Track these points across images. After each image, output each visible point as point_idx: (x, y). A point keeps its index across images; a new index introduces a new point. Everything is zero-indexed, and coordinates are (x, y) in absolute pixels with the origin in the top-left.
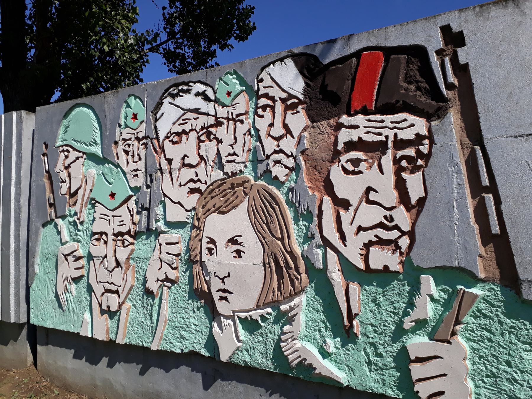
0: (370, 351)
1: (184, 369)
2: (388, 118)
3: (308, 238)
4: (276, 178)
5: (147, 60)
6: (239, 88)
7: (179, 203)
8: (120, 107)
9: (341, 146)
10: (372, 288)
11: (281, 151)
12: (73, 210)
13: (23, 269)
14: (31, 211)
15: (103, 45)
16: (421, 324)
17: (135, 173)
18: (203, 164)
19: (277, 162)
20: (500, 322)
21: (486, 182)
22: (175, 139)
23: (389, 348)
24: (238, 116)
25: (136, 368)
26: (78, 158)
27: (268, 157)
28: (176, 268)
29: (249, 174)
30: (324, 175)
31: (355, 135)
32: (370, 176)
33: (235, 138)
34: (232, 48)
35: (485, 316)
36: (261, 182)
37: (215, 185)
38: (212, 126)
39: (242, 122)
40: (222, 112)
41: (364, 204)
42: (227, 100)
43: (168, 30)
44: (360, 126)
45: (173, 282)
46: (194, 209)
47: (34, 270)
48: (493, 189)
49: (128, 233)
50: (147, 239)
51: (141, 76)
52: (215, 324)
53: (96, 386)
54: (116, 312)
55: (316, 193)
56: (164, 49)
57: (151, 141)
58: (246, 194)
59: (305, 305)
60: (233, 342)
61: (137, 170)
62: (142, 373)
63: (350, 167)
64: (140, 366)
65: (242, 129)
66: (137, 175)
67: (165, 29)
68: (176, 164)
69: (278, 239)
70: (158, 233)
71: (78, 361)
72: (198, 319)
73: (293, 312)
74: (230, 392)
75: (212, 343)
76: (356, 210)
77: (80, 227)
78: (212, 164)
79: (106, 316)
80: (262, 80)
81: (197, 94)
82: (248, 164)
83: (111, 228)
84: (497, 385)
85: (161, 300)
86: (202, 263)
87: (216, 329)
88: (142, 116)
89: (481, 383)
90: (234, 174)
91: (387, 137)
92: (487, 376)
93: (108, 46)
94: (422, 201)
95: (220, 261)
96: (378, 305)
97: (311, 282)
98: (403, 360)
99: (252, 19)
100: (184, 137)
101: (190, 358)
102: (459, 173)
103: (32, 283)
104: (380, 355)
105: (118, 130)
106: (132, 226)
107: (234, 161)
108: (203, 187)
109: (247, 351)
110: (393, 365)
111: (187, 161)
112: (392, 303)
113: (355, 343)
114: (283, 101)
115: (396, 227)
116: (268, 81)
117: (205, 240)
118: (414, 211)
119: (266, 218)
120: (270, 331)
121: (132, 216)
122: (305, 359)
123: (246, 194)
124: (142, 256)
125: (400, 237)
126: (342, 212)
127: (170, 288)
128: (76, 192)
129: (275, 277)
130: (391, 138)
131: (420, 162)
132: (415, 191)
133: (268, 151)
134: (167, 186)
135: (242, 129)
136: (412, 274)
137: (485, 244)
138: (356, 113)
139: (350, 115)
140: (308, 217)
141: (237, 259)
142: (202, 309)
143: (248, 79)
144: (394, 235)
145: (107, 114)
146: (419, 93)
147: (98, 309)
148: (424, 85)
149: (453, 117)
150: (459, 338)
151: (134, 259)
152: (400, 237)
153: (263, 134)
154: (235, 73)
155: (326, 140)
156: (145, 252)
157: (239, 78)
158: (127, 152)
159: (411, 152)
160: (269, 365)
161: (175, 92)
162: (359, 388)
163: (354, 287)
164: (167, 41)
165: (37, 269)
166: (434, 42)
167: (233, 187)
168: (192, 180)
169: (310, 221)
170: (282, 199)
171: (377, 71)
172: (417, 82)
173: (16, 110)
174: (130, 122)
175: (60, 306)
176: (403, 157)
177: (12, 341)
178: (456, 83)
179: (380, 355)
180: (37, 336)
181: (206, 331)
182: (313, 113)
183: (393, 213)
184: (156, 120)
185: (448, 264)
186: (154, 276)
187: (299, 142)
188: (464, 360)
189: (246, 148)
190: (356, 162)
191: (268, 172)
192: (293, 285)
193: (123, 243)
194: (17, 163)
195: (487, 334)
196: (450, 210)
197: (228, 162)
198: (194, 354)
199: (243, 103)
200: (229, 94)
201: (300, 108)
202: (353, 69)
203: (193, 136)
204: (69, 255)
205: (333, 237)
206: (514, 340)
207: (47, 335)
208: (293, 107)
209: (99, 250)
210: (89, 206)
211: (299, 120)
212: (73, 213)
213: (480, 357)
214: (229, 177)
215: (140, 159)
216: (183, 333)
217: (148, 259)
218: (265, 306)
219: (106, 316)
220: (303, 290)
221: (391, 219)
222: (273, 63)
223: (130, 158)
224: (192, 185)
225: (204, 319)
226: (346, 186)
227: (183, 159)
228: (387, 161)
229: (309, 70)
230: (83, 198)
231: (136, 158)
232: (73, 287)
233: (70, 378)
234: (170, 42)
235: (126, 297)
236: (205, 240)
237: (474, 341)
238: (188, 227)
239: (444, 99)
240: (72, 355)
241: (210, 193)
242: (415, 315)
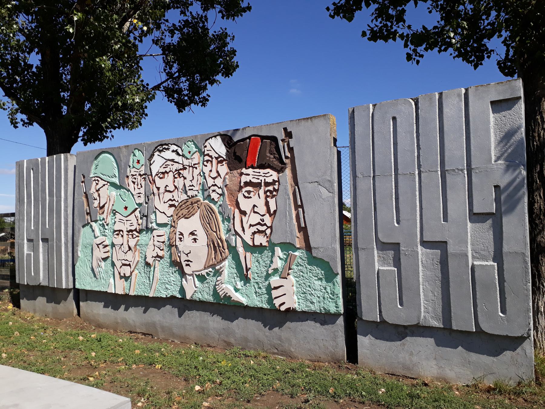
0: (256, 286)
1: (168, 307)
2: (262, 171)
3: (229, 231)
4: (213, 199)
6: (195, 150)
7: (164, 213)
8: (130, 155)
9: (242, 184)
10: (256, 255)
11: (215, 185)
12: (102, 217)
13: (70, 255)
14: (75, 217)
15: (118, 101)
16: (276, 270)
17: (139, 195)
18: (176, 190)
19: (214, 191)
20: (306, 268)
21: (299, 203)
22: (161, 176)
23: (264, 284)
24: (194, 165)
25: (141, 309)
26: (104, 185)
27: (209, 188)
28: (162, 250)
29: (200, 197)
30: (236, 198)
32: (255, 200)
33: (193, 177)
34: (220, 83)
35: (301, 265)
36: (206, 201)
37: (183, 202)
38: (181, 169)
39: (196, 168)
40: (186, 162)
41: (252, 213)
42: (188, 156)
43: (167, 71)
44: (250, 174)
45: (161, 258)
46: (172, 216)
47: (77, 255)
48: (302, 206)
49: (135, 230)
50: (146, 233)
52: (184, 280)
53: (117, 323)
54: (129, 277)
55: (232, 208)
56: (164, 87)
57: (147, 176)
58: (199, 208)
59: (227, 266)
60: (193, 289)
61: (140, 193)
62: (145, 312)
63: (246, 195)
64: (144, 308)
65: (196, 172)
66: (140, 196)
67: (165, 70)
68: (162, 190)
69: (214, 232)
70: (152, 230)
71: (106, 309)
72: (175, 277)
73: (222, 270)
74: (192, 317)
75: (182, 290)
76: (249, 216)
77: (106, 227)
78: (181, 191)
79: (123, 279)
80: (206, 147)
81: (173, 151)
82: (200, 191)
83: (125, 227)
84: (305, 297)
85: (154, 268)
86: (176, 246)
87: (184, 281)
88: (142, 162)
89: (300, 297)
90: (192, 197)
91: (261, 180)
92: (302, 293)
93: (121, 102)
94: (275, 212)
95: (185, 245)
96: (259, 263)
97: (230, 253)
98: (269, 289)
99: (235, 59)
100: (166, 175)
101: (171, 300)
102: (289, 199)
103: (77, 262)
104: (260, 288)
105: (128, 169)
106: (138, 226)
107: (192, 189)
108: (176, 204)
109: (200, 292)
110: (265, 292)
111: (168, 189)
112: (264, 262)
113: (250, 283)
114: (217, 158)
115: (265, 224)
117: (178, 233)
118: (273, 216)
119: (208, 221)
120: (212, 280)
121: (137, 220)
122: (227, 293)
123: (199, 208)
124: (143, 244)
125: (266, 229)
126: (243, 217)
127: (159, 261)
128: (104, 206)
129: (213, 252)
130: (263, 181)
131: (274, 193)
132: (273, 208)
133: (209, 185)
134: (157, 202)
135: (196, 172)
136: (272, 246)
137: (299, 232)
138: (249, 168)
139: (246, 169)
140: (228, 220)
141: (195, 243)
142: (177, 272)
143: (199, 145)
144: (264, 228)
145: (122, 159)
146: (274, 160)
147: (118, 276)
148: (277, 156)
149: (288, 172)
150: (291, 277)
151: (139, 245)
152: (266, 229)
154: (193, 141)
155: (236, 180)
156: (145, 241)
157: (195, 144)
158: (134, 183)
159: (271, 188)
160: (211, 299)
161: (161, 149)
162: (252, 306)
163: (248, 255)
164: (167, 80)
165: (79, 254)
166: (280, 135)
167: (192, 204)
168: (170, 200)
169: (229, 222)
170: (216, 210)
171: (257, 147)
172: (274, 154)
173: (63, 153)
174: (136, 165)
175: (95, 276)
176: (268, 191)
177: (63, 301)
178: (289, 156)
179: (260, 288)
180: (80, 295)
181: (179, 284)
182: (230, 166)
183: (264, 217)
184: (151, 165)
185: (285, 241)
186: (150, 254)
187: (224, 181)
188: (293, 286)
189: (199, 183)
190: (249, 192)
191: (209, 196)
192: (221, 256)
193: (133, 236)
194: (65, 187)
195: (302, 274)
196: (286, 216)
197: (190, 190)
198: (173, 297)
199: (196, 159)
200: (190, 152)
201: (224, 162)
202: (247, 145)
203: (171, 174)
204: (100, 244)
205: (239, 230)
206: (311, 276)
207: (86, 295)
208: (221, 162)
209: (118, 240)
210: (112, 214)
211: (224, 169)
212: (102, 219)
213: (299, 285)
214: (190, 198)
215: (142, 187)
216: (167, 286)
217: (147, 245)
218: (209, 267)
219: (123, 279)
220: (226, 258)
221: (263, 220)
222: (211, 138)
223: (136, 186)
224: (170, 202)
225: (179, 277)
226: (245, 205)
227: (166, 187)
228: (262, 192)
229: (228, 144)
230: (108, 209)
231: (139, 186)
232: (103, 264)
233: (101, 320)
234: (169, 81)
235: (135, 268)
236: (178, 233)
237: (297, 277)
238: (169, 226)
239: (285, 164)
240: (102, 306)
241: (180, 207)
242: (273, 266)
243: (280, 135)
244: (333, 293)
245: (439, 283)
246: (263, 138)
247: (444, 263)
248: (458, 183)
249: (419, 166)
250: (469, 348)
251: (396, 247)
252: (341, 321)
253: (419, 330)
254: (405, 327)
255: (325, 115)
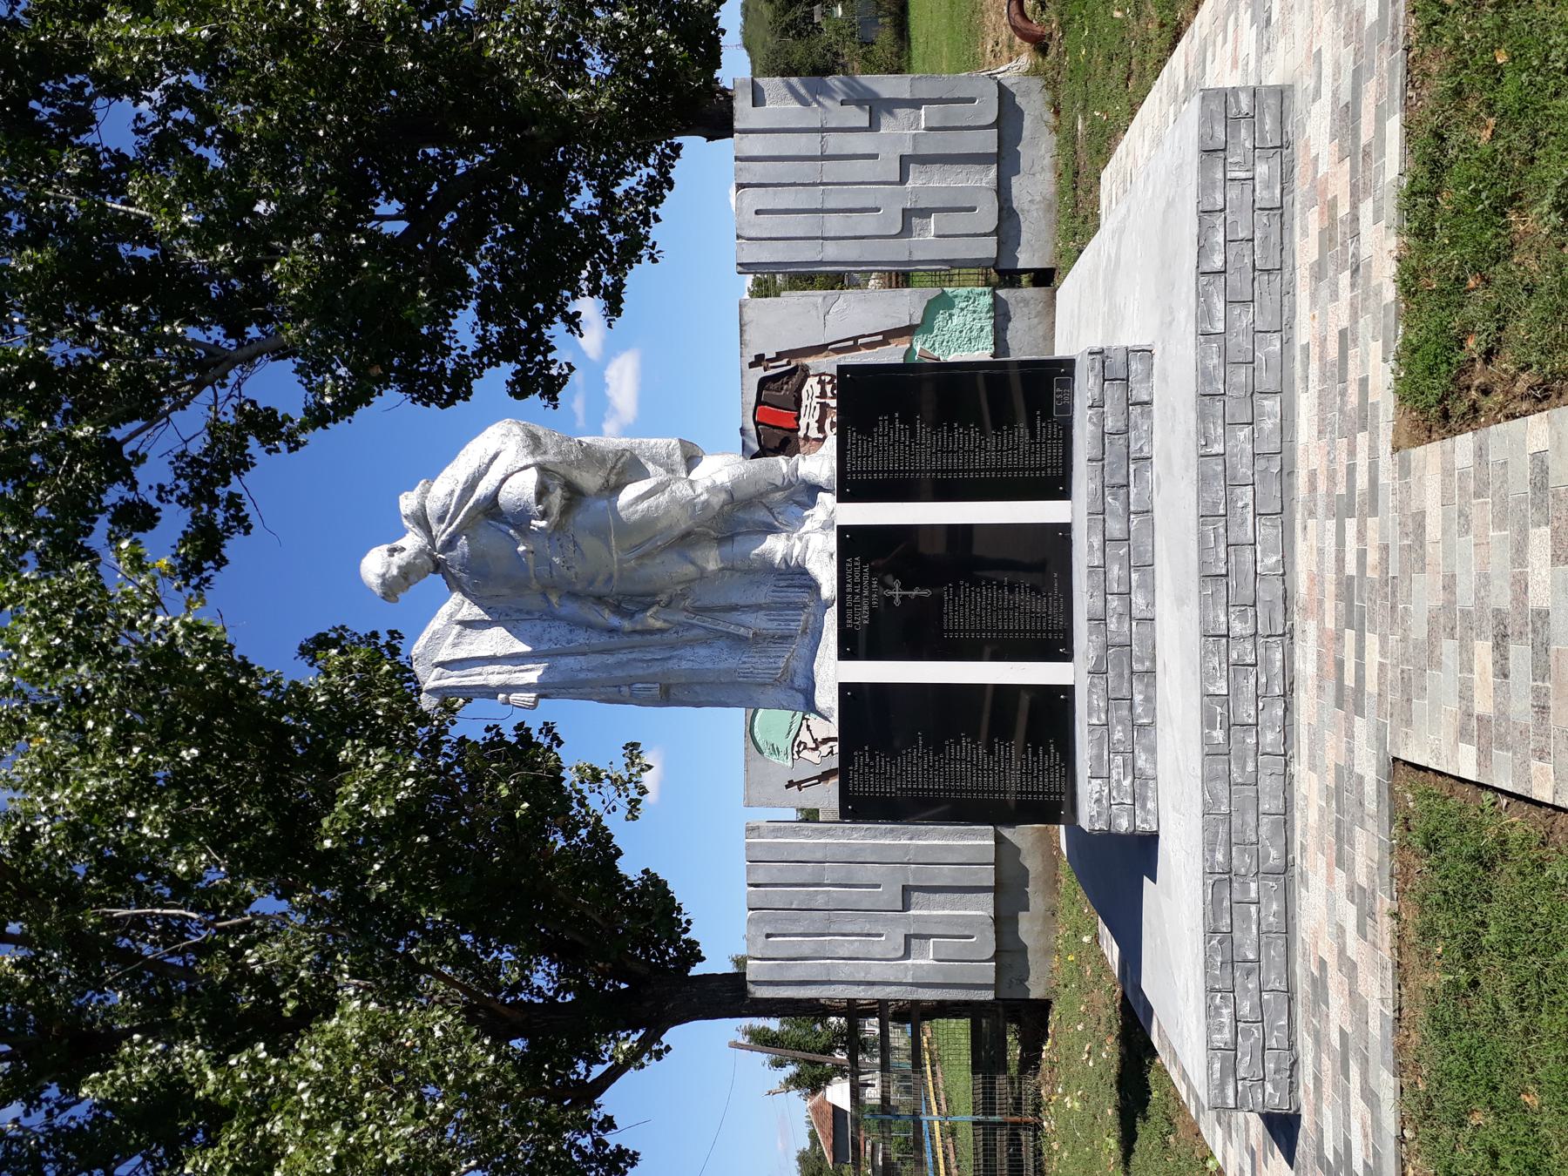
2: (805, 402)
31: (814, 425)
48: (855, 339)
166: (760, 372)
239: (796, 368)
243: (760, 372)
244: (967, 298)
245: (947, 167)
246: (759, 402)
247: (925, 160)
248: (835, 143)
249: (814, 184)
250: (1018, 138)
251: (907, 214)
252: (1007, 832)
253: (1004, 923)
254: (1000, 210)
255: (740, 306)
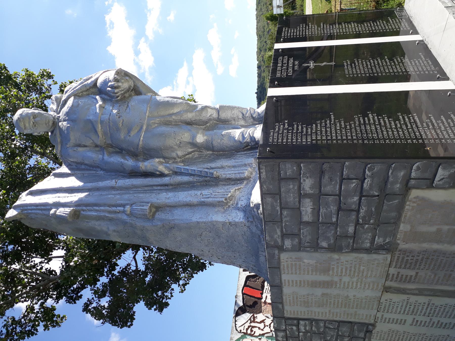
5: (88, 301)
51: (77, 301)
80: (241, 331)
116: (242, 328)
138: (262, 296)
139: (262, 298)
153: (262, 332)
182: (258, 312)
201: (255, 316)
208: (254, 318)
211: (260, 317)
222: (236, 325)
